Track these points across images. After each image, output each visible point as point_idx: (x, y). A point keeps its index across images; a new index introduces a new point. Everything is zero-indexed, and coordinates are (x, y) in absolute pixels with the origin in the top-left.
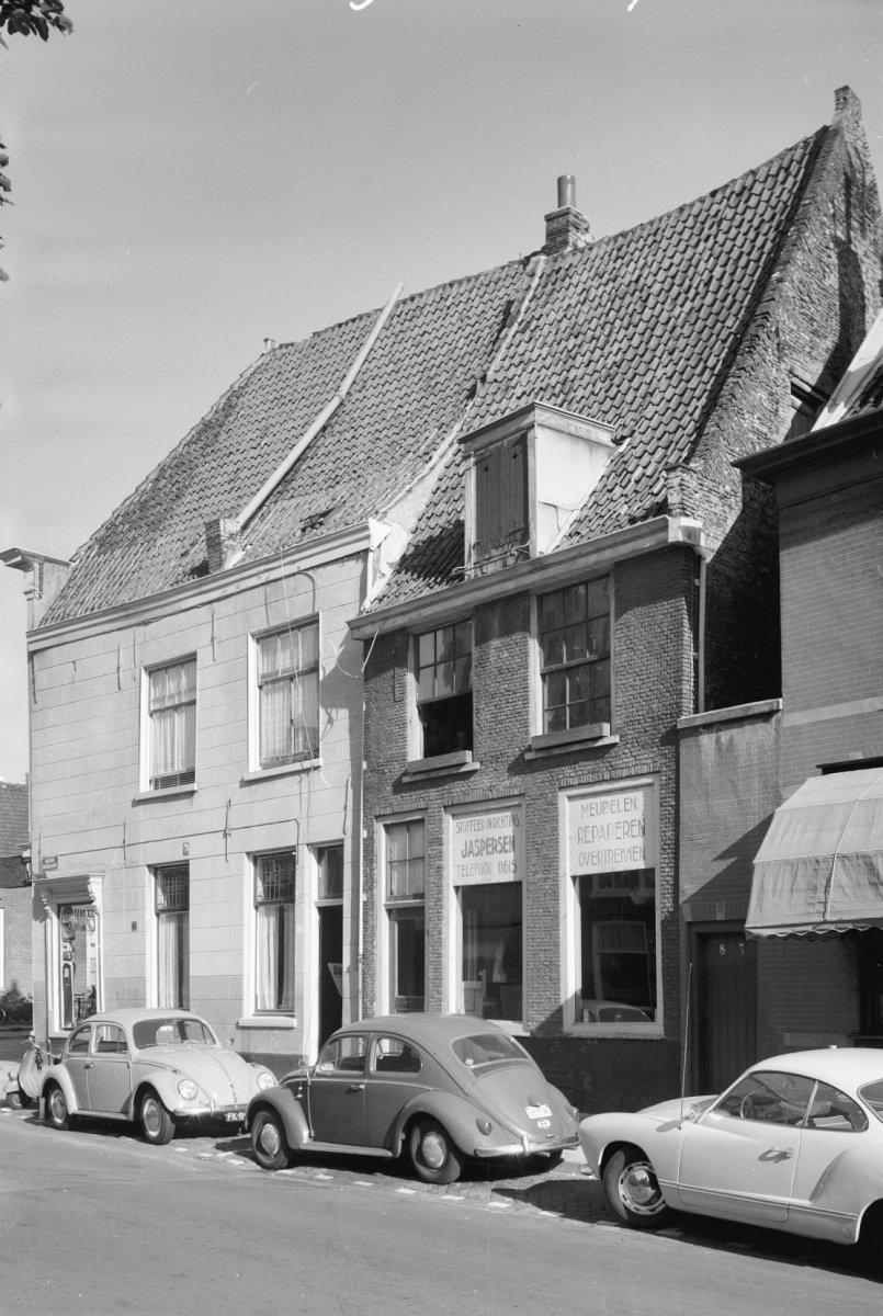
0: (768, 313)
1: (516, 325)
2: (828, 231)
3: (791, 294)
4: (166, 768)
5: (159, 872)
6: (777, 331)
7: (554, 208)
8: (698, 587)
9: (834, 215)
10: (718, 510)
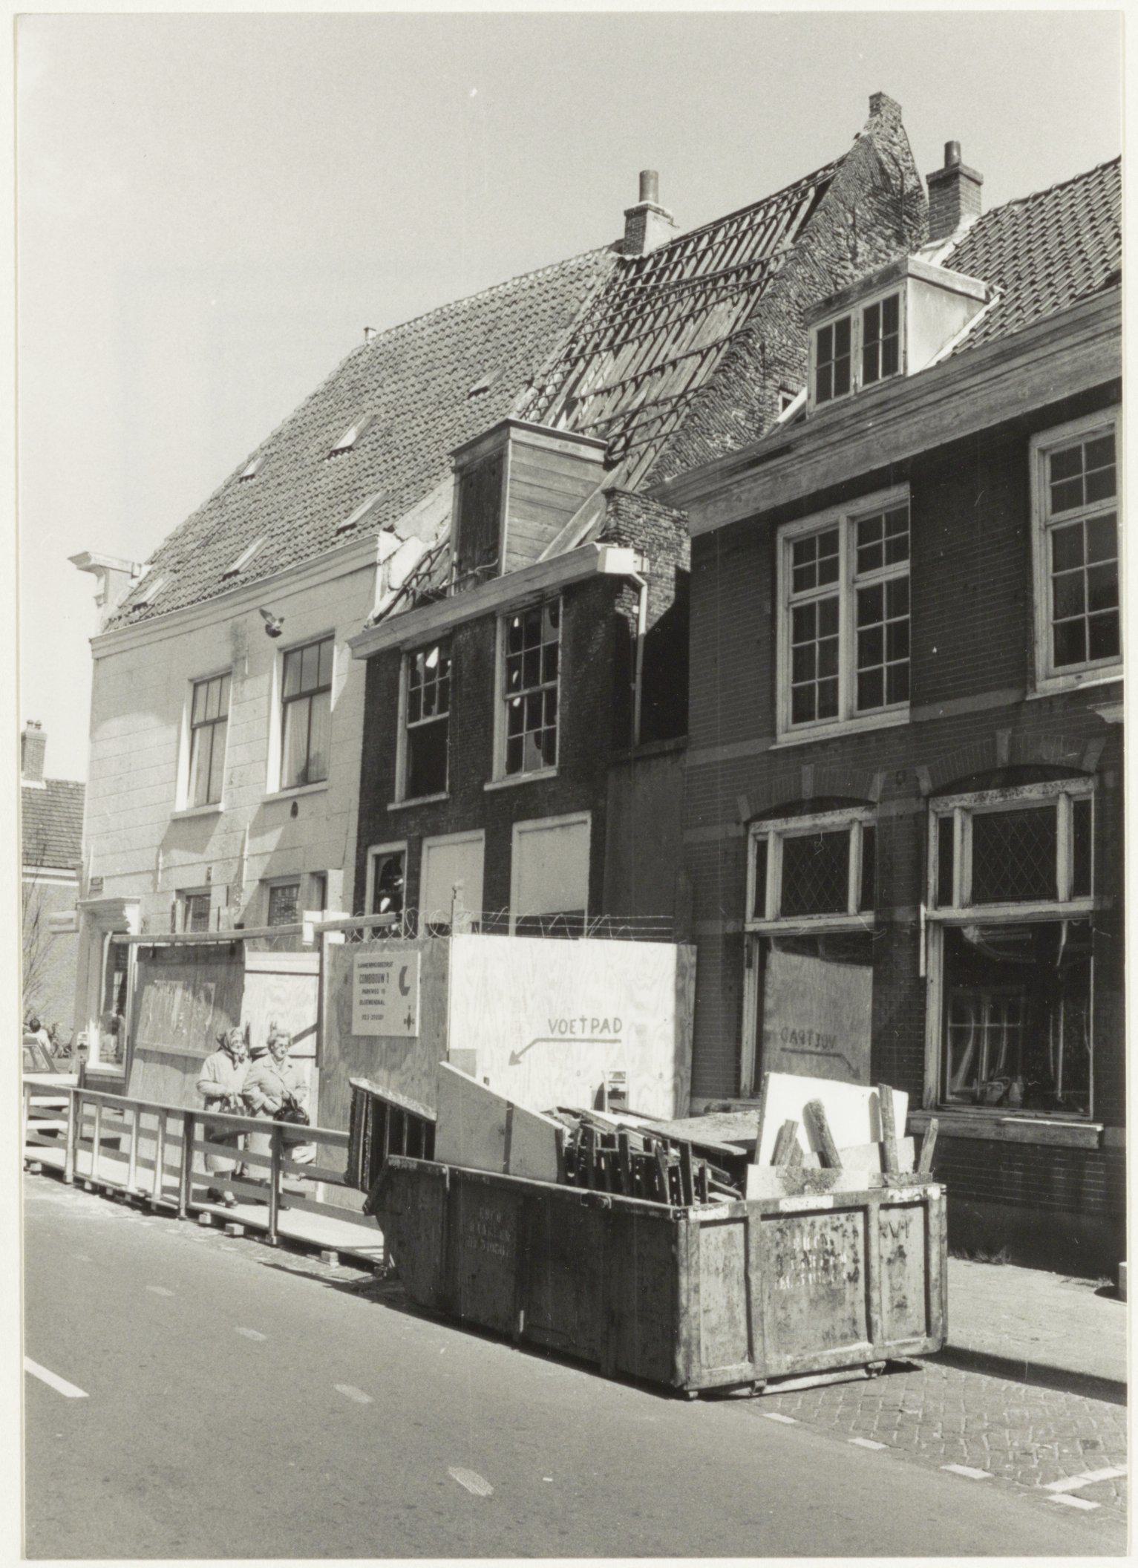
0: (751, 330)
1: (555, 352)
2: (844, 243)
3: (784, 308)
4: (365, 966)
5: (192, 900)
6: (763, 348)
7: (635, 204)
8: (638, 615)
9: (854, 225)
10: (670, 534)
